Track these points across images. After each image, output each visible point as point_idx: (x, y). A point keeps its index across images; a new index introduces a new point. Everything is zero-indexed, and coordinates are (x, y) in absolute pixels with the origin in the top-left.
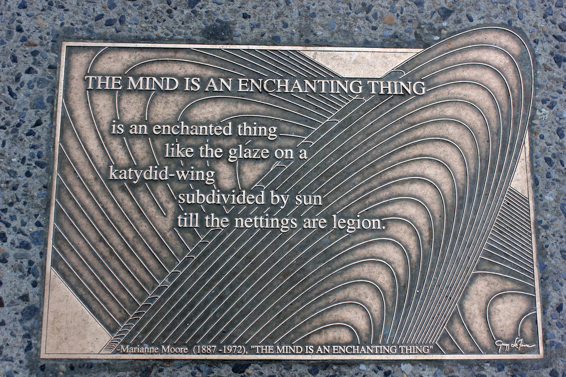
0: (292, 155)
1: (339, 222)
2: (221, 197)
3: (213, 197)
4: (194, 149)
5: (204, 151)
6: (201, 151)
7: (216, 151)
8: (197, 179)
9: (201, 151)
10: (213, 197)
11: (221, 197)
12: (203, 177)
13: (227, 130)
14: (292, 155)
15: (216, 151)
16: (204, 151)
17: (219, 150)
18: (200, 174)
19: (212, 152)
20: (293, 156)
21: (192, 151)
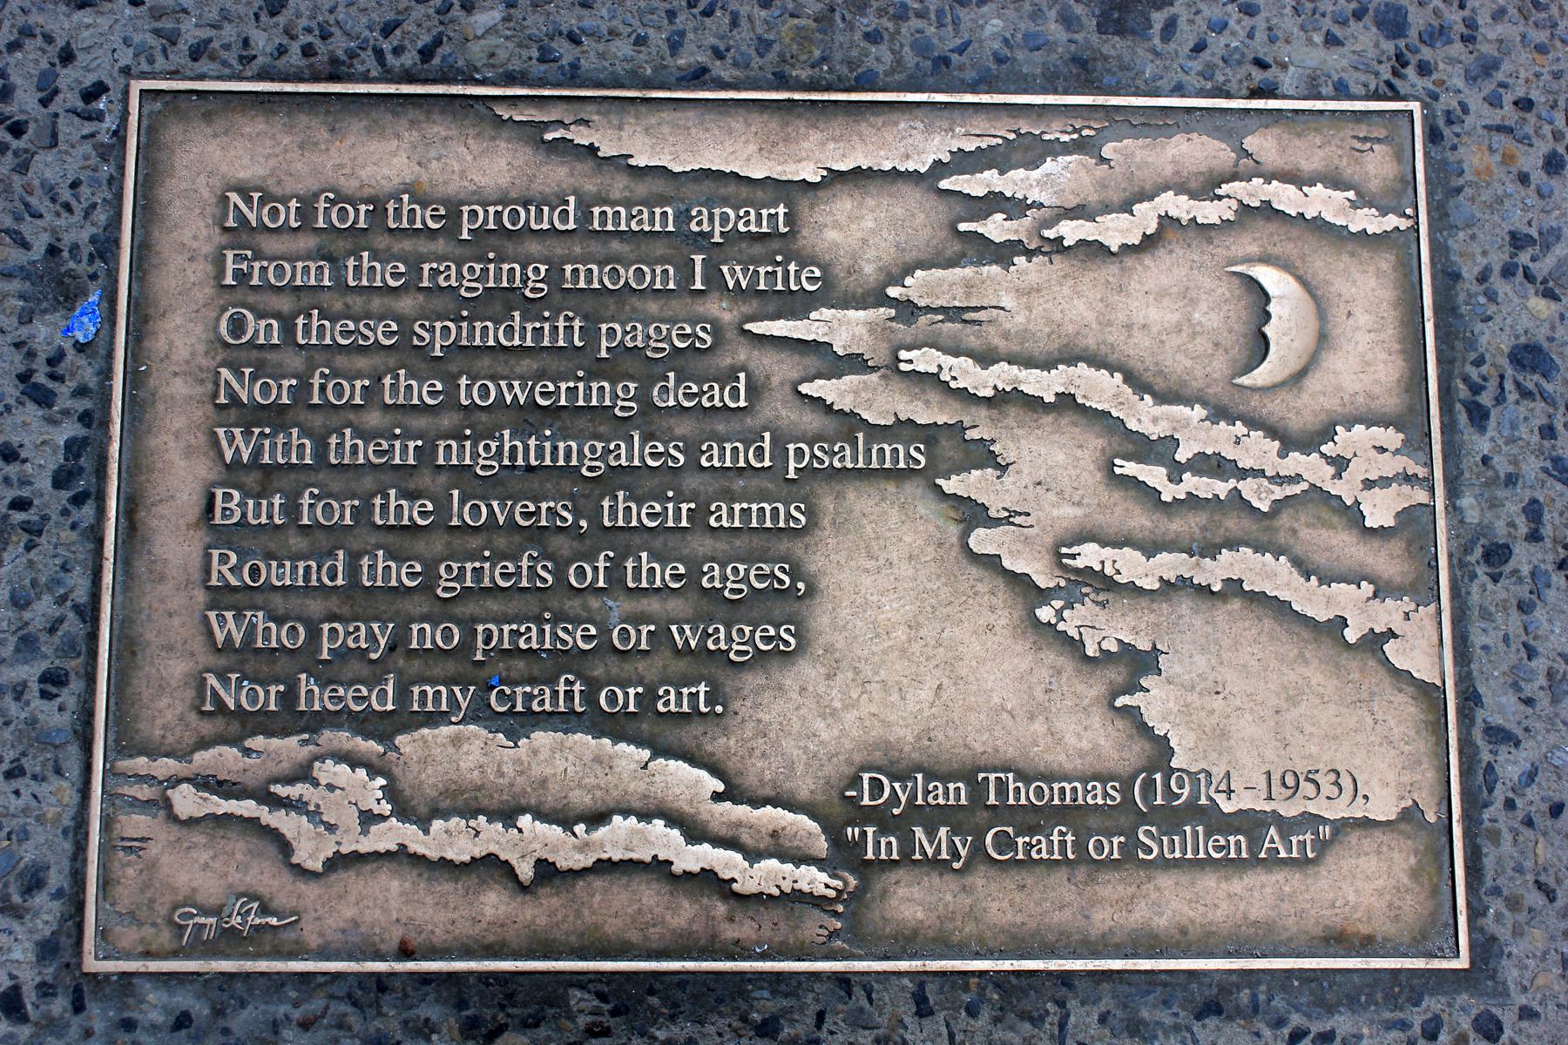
0: (275, 334)
1: (647, 450)
2: (451, 693)
3: (717, 223)
4: (405, 263)
5: (394, 387)
6: (300, 327)
7: (425, 389)
8: (594, 403)
9: (300, 327)
10: (717, 223)
11: (451, 693)
12: (607, 396)
13: (383, 694)
14: (275, 334)
15: (371, 448)
16: (394, 387)
17: (424, 505)
18: (568, 450)
19: (596, 273)
20: (705, 281)
21: (402, 269)
